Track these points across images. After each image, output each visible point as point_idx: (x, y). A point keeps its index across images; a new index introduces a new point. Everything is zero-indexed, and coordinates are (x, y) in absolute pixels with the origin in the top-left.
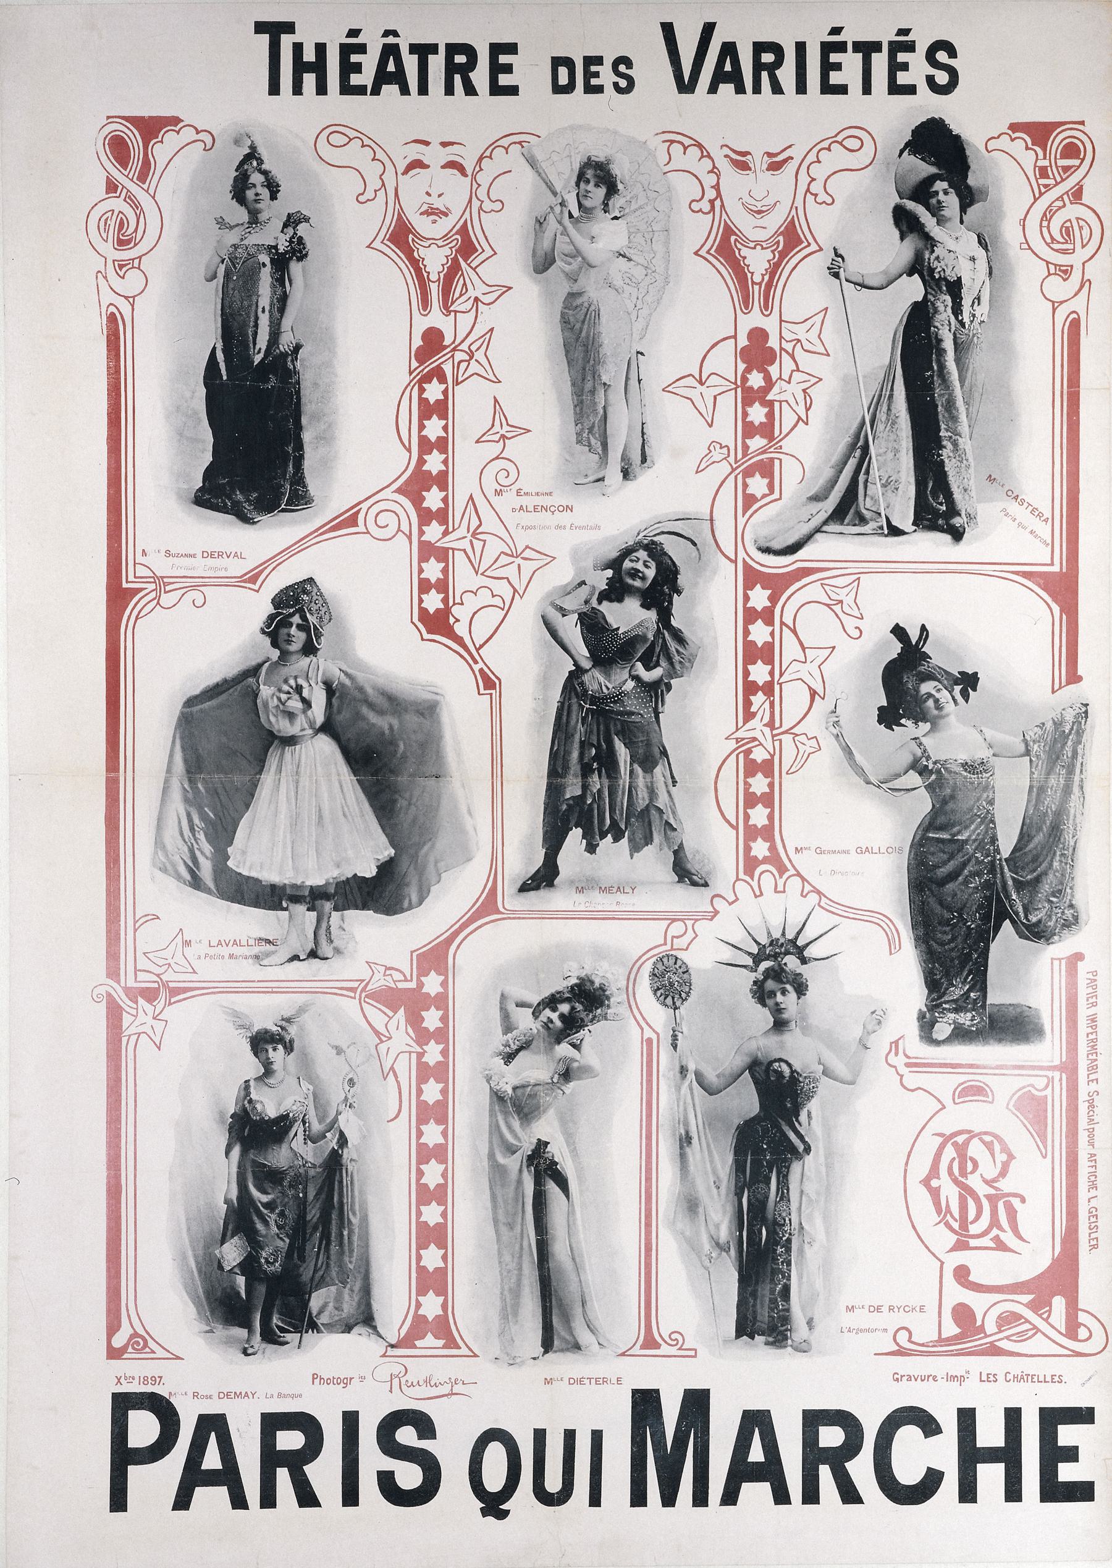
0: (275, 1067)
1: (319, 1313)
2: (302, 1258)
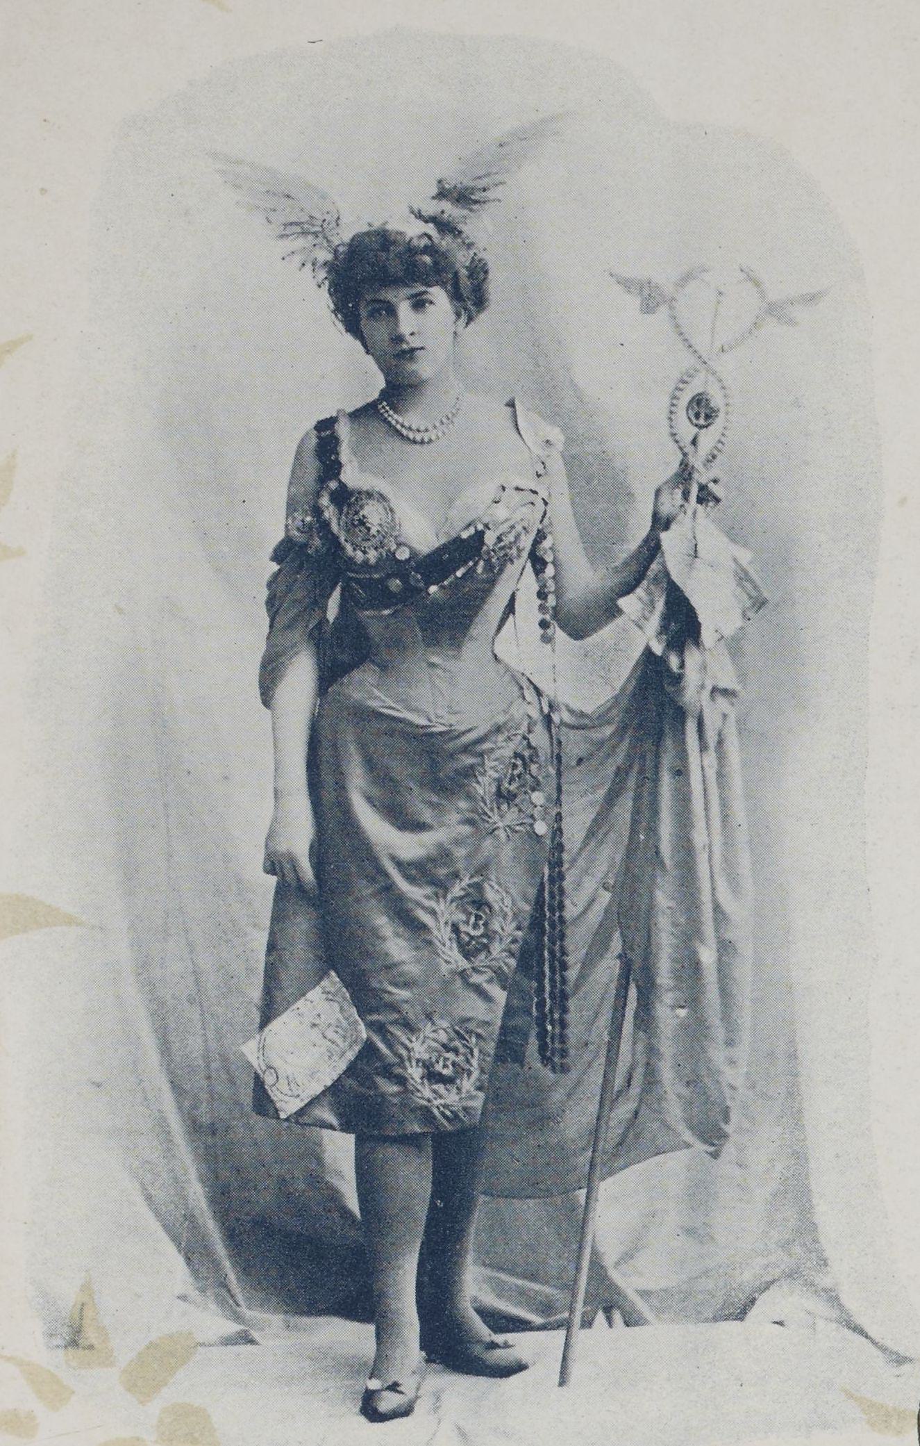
0: (424, 367)
1: (627, 1256)
2: (555, 1054)
